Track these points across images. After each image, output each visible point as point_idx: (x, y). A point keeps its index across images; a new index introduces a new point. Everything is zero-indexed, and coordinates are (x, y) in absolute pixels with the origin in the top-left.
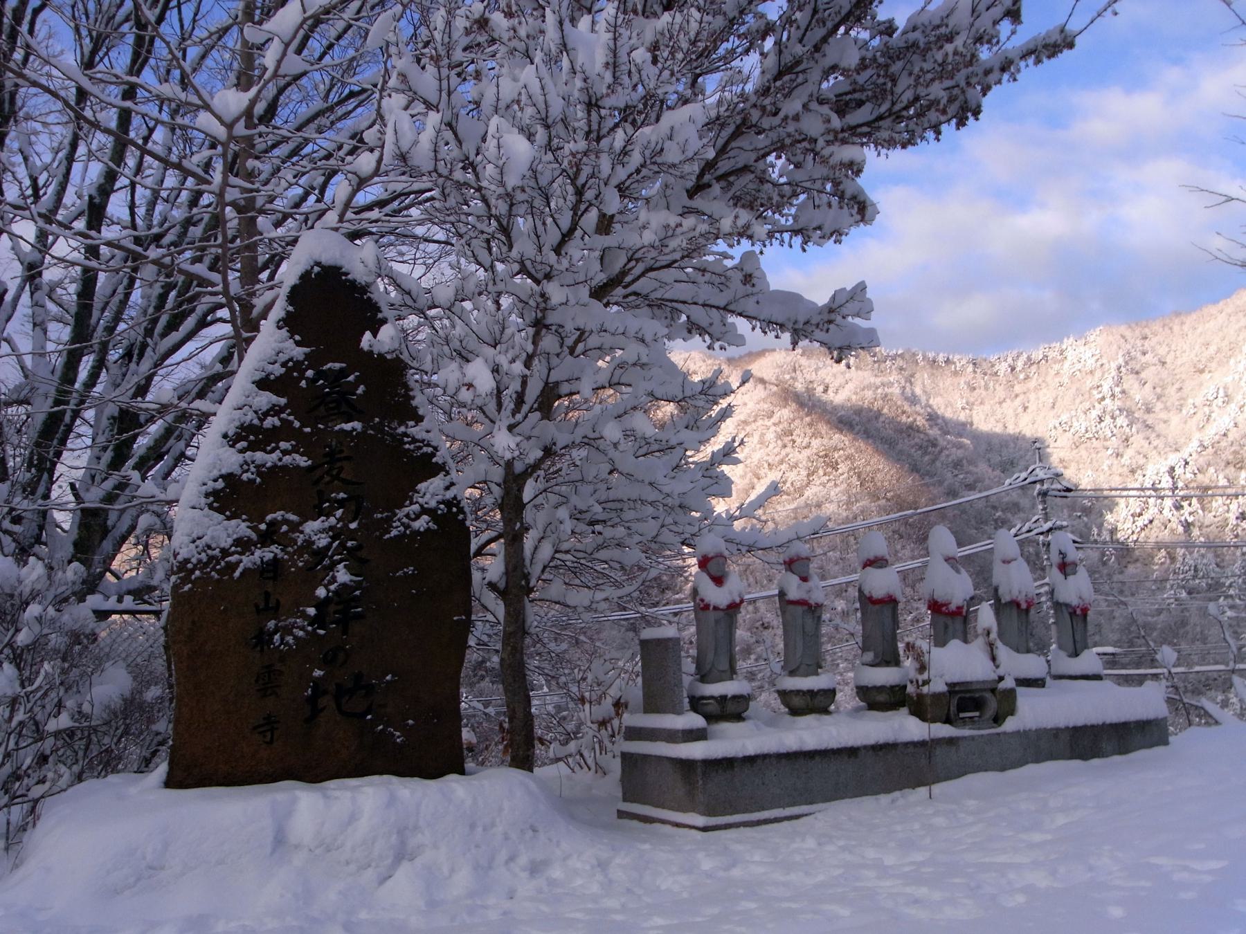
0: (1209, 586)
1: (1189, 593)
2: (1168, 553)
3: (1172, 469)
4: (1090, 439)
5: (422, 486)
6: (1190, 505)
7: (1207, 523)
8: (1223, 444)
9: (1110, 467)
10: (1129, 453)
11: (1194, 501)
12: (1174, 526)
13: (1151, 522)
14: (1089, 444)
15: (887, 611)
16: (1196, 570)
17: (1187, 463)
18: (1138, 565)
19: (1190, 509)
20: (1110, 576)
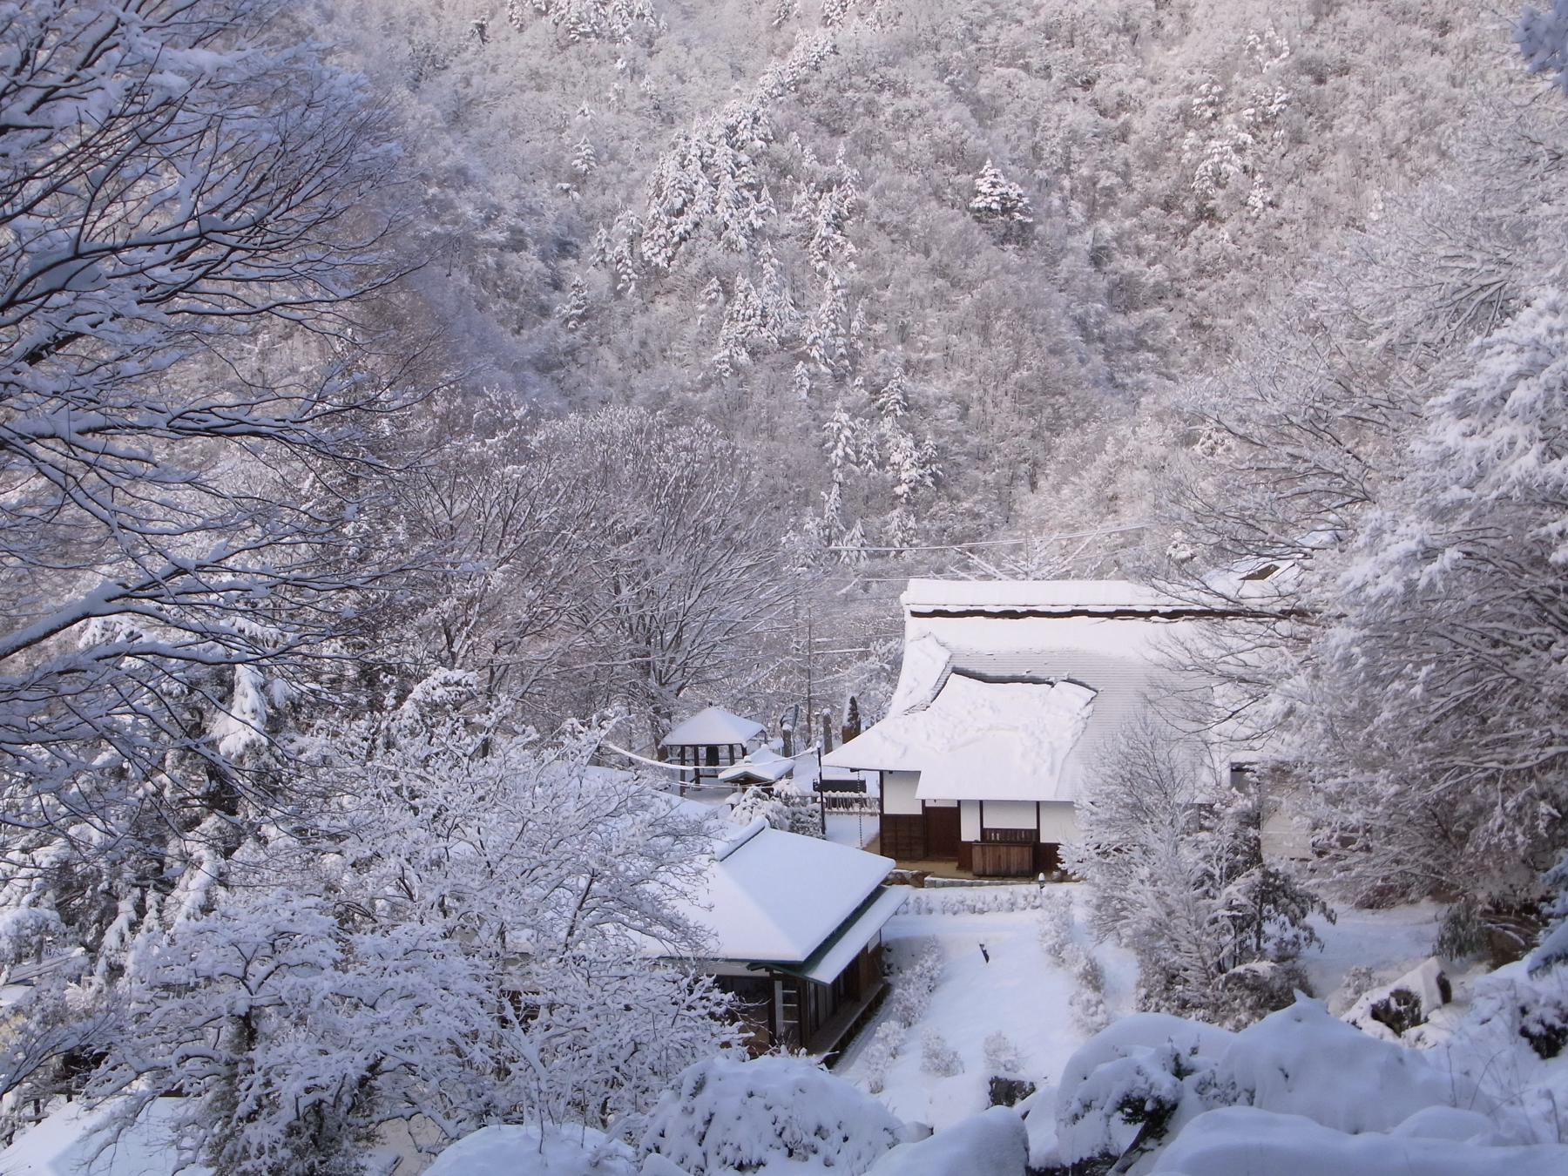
0: (782, 342)
1: (752, 354)
2: (722, 283)
3: (733, 129)
4: (586, 35)
5: (964, 838)
6: (758, 199)
7: (783, 231)
8: (814, 87)
9: (620, 95)
10: (656, 66)
11: (765, 193)
12: (733, 236)
13: (696, 225)
14: (583, 46)
15: (886, 776)
16: (764, 315)
17: (756, 120)
18: (673, 298)
19: (758, 207)
20: (627, 318)
